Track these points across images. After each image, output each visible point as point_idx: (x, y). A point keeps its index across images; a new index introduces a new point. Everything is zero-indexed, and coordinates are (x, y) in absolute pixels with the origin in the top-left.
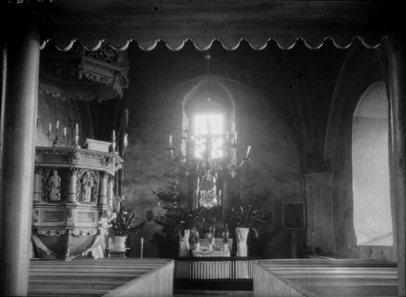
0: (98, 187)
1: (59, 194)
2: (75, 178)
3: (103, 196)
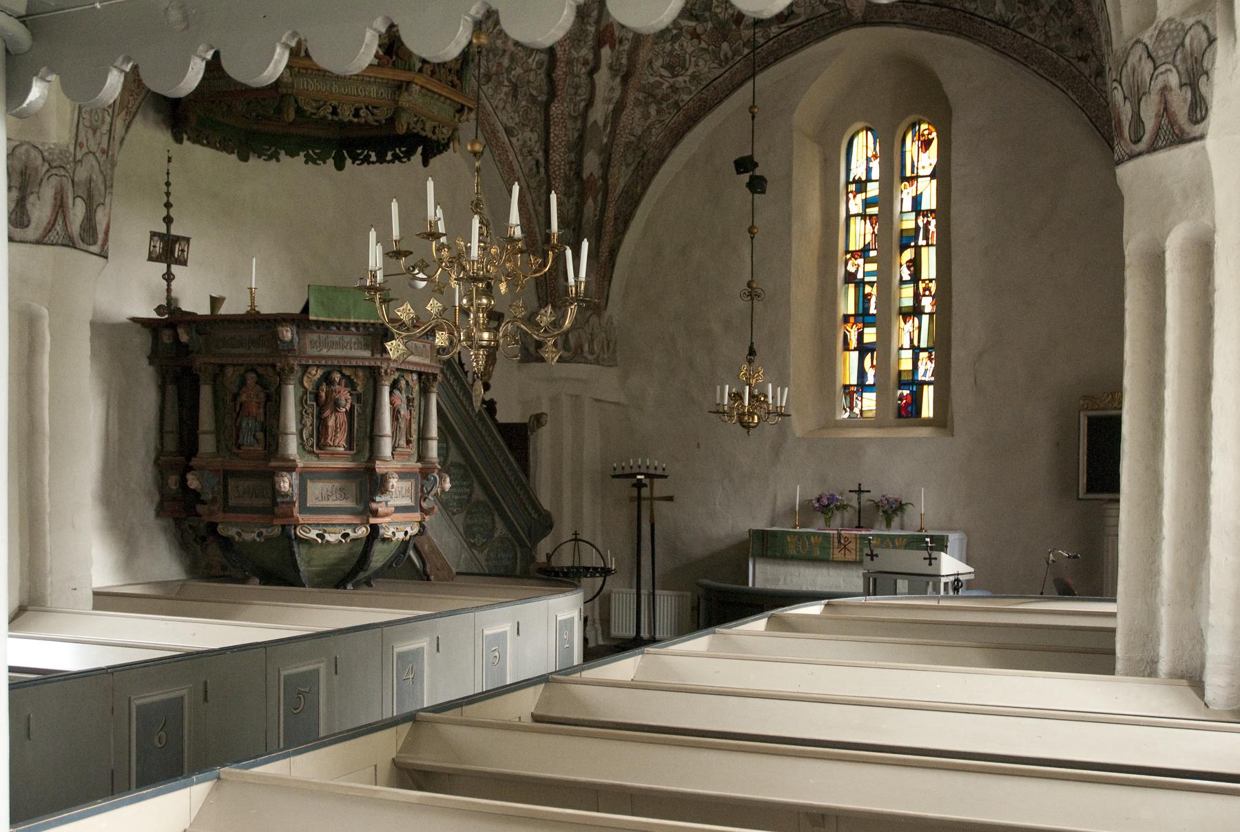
1: (260, 435)
3: (432, 439)
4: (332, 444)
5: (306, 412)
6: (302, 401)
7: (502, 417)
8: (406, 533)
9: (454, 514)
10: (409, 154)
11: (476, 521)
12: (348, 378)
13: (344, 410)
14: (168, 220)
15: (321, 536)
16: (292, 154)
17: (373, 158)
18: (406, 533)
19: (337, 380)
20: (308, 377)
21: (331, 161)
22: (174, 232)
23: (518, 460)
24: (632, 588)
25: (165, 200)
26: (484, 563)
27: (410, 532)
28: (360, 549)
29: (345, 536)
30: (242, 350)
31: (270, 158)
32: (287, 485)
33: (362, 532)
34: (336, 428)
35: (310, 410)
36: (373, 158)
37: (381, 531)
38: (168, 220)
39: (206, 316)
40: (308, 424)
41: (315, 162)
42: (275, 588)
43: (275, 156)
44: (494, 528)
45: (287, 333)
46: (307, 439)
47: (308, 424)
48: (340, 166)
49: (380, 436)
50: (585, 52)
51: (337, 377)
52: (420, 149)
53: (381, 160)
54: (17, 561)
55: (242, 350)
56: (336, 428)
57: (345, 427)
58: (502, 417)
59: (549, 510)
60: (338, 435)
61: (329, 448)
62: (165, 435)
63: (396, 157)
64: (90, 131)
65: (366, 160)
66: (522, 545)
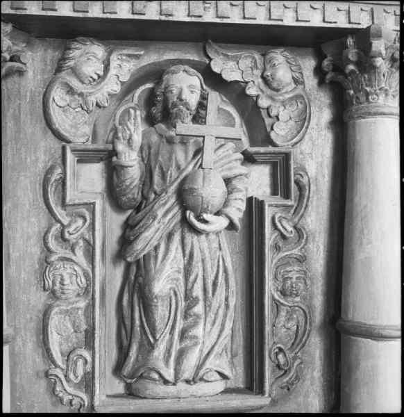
0: (317, 218)
2: (29, 188)
4: (169, 374)
5: (62, 237)
6: (46, 182)
12: (235, 92)
13: (222, 222)
19: (193, 99)
20: (71, 91)
24: (233, 126)
34: (190, 300)
35: (77, 229)
39: (270, 170)
40: (71, 287)
46: (67, 356)
47: (71, 287)
49: (372, 57)
50: (299, 374)
51: (187, 85)
54: (244, 285)
56: (190, 300)
57: (230, 296)
60: (199, 331)
61: (161, 389)
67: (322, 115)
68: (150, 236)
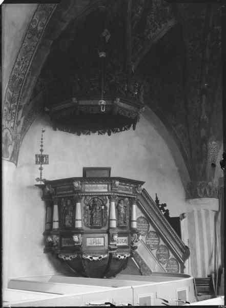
3: (77, 220)
7: (171, 215)
8: (125, 256)
9: (152, 250)
10: (129, 127)
11: (161, 252)
12: (101, 199)
14: (42, 150)
15: (91, 258)
16: (94, 132)
17: (119, 130)
18: (125, 256)
21: (106, 134)
22: (43, 154)
23: (176, 231)
25: (40, 148)
26: (165, 269)
27: (127, 256)
28: (106, 262)
29: (100, 257)
30: (65, 192)
31: (87, 134)
32: (77, 239)
33: (76, 256)
36: (119, 130)
37: (113, 256)
38: (42, 150)
41: (101, 134)
42: (90, 286)
43: (89, 133)
44: (169, 256)
45: (76, 184)
48: (109, 134)
51: (96, 199)
52: (132, 125)
53: (121, 131)
55: (65, 192)
58: (171, 215)
59: (187, 245)
62: (112, 260)
63: (125, 129)
64: (7, 122)
65: (117, 131)
66: (181, 262)
67: (108, 201)
68: (93, 212)
